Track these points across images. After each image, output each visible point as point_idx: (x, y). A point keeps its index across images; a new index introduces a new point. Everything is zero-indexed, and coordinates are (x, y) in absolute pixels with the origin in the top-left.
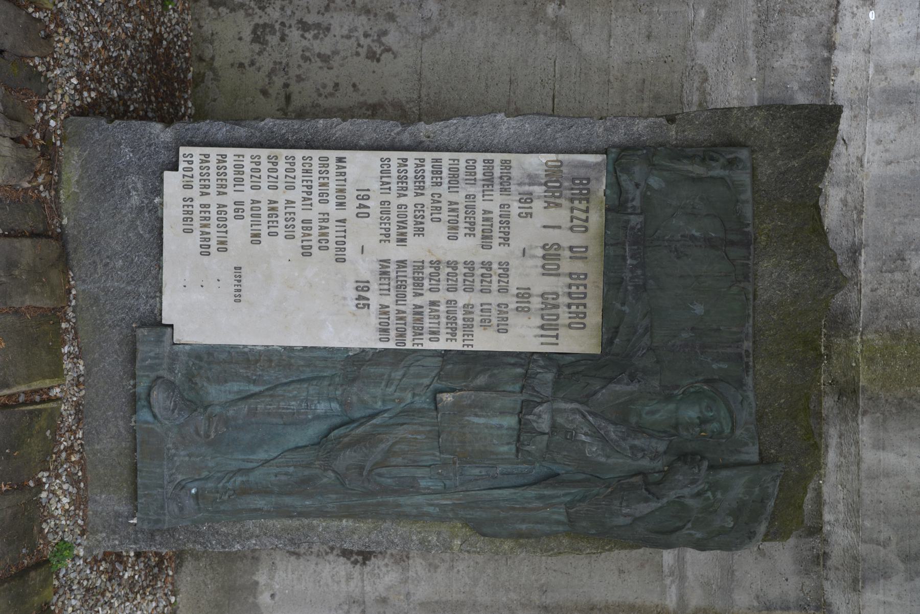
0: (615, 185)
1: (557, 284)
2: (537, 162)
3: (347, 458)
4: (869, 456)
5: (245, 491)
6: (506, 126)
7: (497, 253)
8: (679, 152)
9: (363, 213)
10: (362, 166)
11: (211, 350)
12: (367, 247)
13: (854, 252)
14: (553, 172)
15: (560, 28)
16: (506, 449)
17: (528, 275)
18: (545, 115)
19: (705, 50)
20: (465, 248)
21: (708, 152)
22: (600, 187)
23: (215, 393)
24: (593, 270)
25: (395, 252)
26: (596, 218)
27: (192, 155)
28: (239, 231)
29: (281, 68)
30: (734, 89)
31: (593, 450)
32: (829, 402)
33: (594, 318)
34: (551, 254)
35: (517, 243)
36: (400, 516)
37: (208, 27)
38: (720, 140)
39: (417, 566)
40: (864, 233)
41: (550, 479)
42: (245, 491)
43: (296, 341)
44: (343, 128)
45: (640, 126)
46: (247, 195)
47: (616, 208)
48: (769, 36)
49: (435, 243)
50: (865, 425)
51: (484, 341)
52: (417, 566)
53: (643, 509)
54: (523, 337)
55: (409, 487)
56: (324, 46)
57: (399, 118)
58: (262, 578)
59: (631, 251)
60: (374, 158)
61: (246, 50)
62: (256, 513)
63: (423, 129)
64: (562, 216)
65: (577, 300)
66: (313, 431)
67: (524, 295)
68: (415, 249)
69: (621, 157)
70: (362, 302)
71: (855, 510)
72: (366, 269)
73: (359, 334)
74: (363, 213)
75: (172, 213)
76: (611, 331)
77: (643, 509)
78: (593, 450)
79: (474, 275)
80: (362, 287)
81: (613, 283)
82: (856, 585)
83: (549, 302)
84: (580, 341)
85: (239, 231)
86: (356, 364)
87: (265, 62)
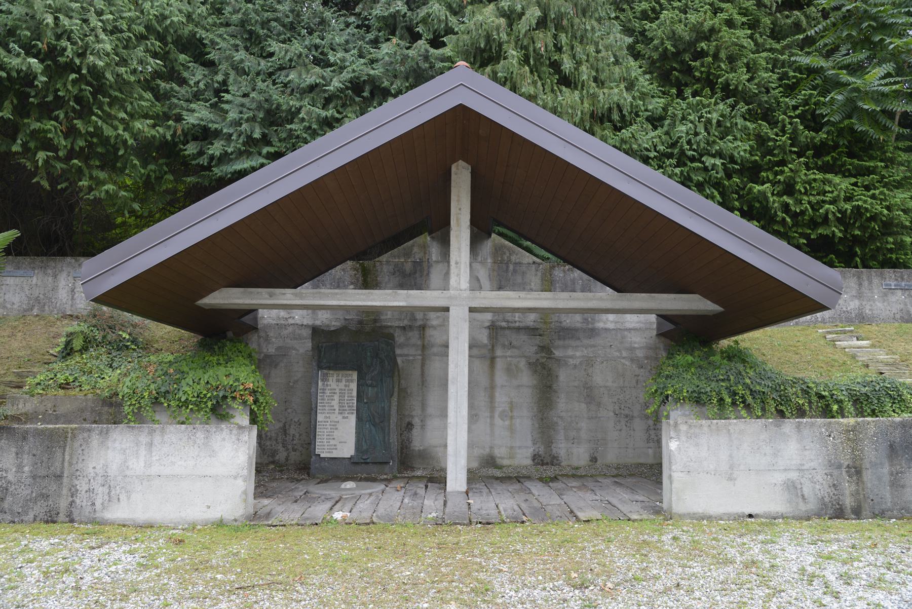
0: (325, 368)
1: (344, 379)
2: (320, 383)
3: (377, 420)
4: (389, 316)
5: (384, 441)
6: (313, 390)
7: (337, 391)
8: (319, 357)
9: (329, 417)
10: (320, 418)
11: (356, 448)
12: (336, 417)
13: (346, 319)
14: (322, 380)
15: (296, 382)
16: (376, 389)
17: (342, 385)
18: (312, 382)
19: (301, 351)
20: (336, 397)
21: (320, 351)
22: (325, 371)
23: (365, 447)
24: (341, 373)
25: (337, 411)
26: (331, 372)
27: (317, 452)
28: (332, 442)
29: (302, 446)
30: (309, 345)
31: (376, 372)
32: (378, 325)
33: (350, 372)
34: (338, 381)
35: (335, 387)
36: (390, 410)
37: (292, 462)
38: (317, 348)
39: (414, 413)
40: (342, 318)
41: (381, 380)
42: (384, 441)
43: (354, 431)
44: (313, 422)
45: (314, 364)
46: (325, 440)
47: (329, 368)
48: (300, 338)
49: (335, 403)
50: (382, 317)
51: (355, 393)
52: (414, 413)
53: (387, 363)
54: (354, 386)
55: (383, 408)
56: (297, 435)
57: (311, 411)
58: (417, 449)
59: (338, 365)
60: (319, 415)
61: (298, 453)
62: (389, 439)
63: (313, 406)
64: (331, 378)
65: (347, 375)
66: (372, 428)
67: (346, 386)
68: (336, 407)
69: (320, 367)
70: (347, 418)
71: (400, 320)
72: (340, 417)
73: (353, 419)
74: (329, 417)
75: (329, 455)
76: (352, 369)
77: (387, 363)
78: (376, 372)
79: (342, 395)
80: (344, 418)
81: (344, 369)
82: (416, 320)
83: (347, 381)
84: (355, 375)
85: (332, 442)
86: (359, 419)
87: (301, 449)
